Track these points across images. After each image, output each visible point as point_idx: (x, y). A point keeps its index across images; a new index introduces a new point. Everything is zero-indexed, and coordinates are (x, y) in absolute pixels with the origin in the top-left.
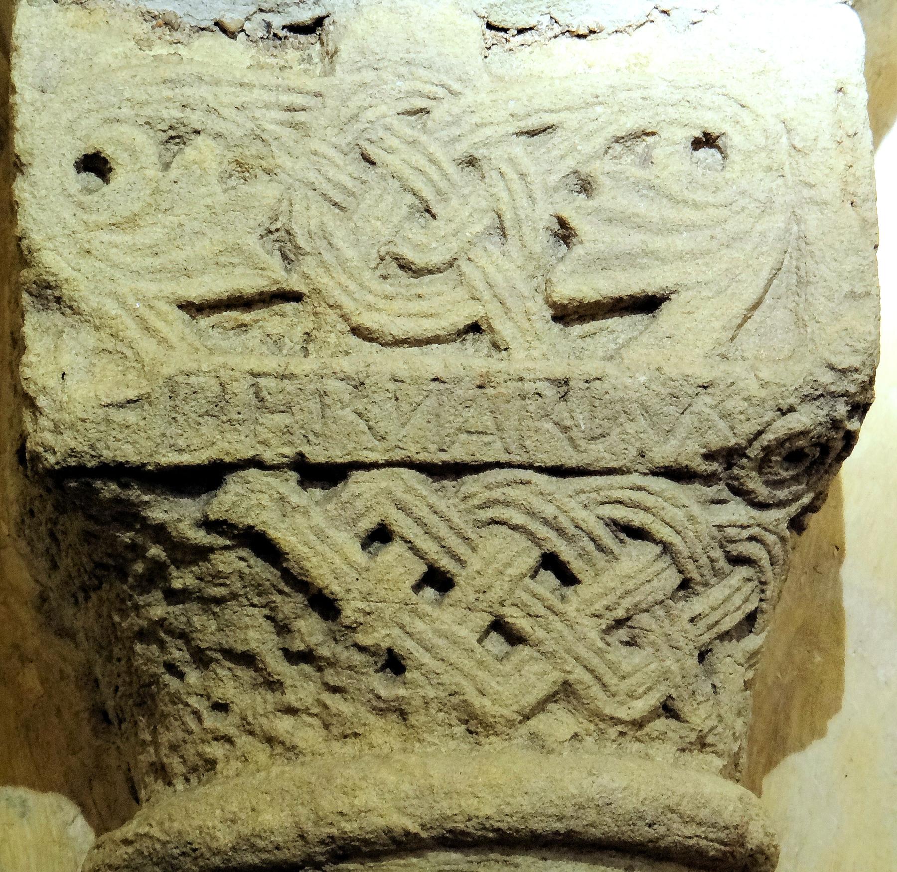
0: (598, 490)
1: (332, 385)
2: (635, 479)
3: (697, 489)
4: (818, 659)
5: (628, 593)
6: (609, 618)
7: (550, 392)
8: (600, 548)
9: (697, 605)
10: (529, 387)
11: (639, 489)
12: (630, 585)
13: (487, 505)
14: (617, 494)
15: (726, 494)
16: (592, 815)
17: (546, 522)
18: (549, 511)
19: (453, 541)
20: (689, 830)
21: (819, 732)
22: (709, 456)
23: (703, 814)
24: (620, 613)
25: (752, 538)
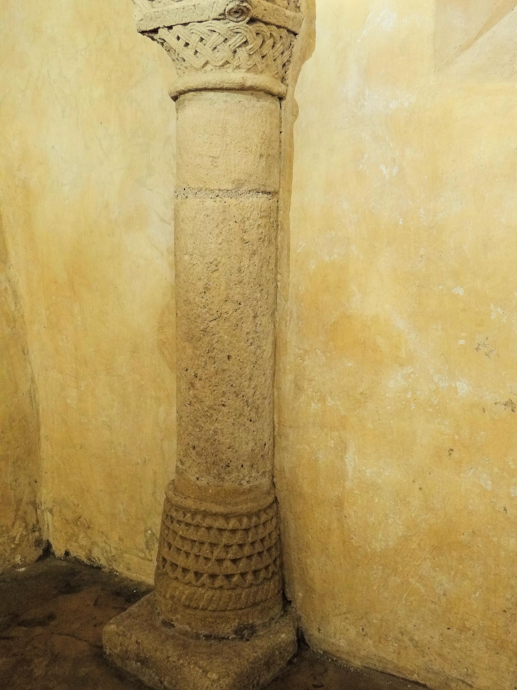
0: (205, 24)
1: (165, 12)
2: (210, 21)
3: (221, 21)
4: (311, 41)
5: (214, 43)
6: (212, 48)
7: (193, 8)
8: (208, 35)
9: (229, 43)
10: (190, 7)
11: (211, 23)
12: (214, 41)
13: (191, 30)
14: (208, 25)
15: (229, 21)
16: (207, 85)
17: (199, 32)
18: (199, 29)
19: (187, 37)
20: (228, 85)
21: (311, 56)
22: (220, 15)
23: (231, 82)
24: (214, 47)
25: (237, 28)
